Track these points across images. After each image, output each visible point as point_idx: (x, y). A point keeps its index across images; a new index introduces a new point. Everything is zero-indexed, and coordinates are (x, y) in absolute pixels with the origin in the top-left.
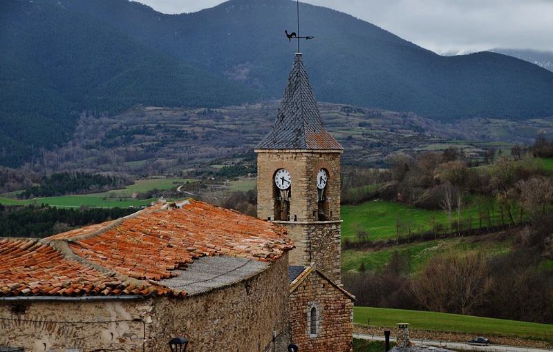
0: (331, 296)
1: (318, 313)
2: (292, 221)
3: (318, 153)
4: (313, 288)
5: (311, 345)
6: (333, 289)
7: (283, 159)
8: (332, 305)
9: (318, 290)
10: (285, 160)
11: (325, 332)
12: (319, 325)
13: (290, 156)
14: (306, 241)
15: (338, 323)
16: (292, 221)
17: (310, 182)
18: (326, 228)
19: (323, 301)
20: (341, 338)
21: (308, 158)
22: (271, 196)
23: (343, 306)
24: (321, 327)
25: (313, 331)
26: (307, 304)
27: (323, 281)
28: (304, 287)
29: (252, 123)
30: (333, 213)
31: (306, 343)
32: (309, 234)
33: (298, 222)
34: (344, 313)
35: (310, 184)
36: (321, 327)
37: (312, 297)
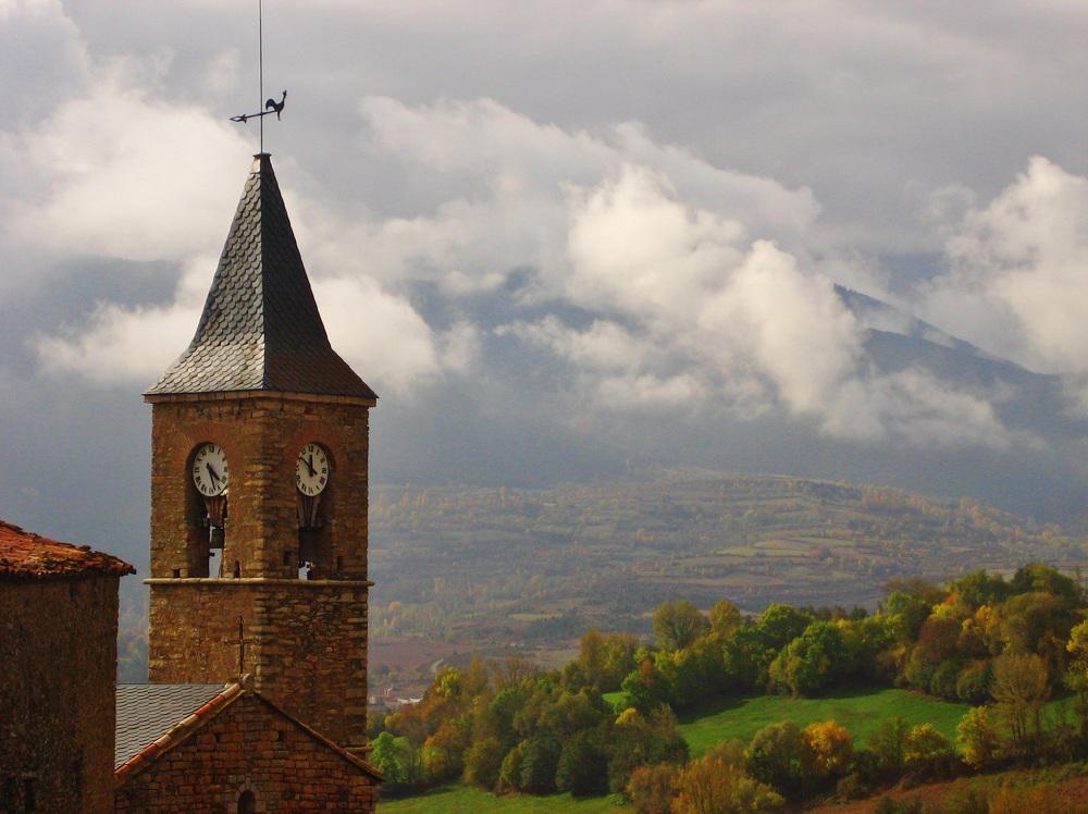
0: (306, 764)
6: (308, 746)
8: (308, 788)
9: (260, 746)
10: (216, 420)
13: (225, 409)
14: (260, 629)
17: (276, 475)
18: (322, 599)
21: (270, 413)
27: (279, 725)
28: (218, 735)
29: (607, 520)
30: (346, 562)
32: (269, 609)
35: (275, 481)
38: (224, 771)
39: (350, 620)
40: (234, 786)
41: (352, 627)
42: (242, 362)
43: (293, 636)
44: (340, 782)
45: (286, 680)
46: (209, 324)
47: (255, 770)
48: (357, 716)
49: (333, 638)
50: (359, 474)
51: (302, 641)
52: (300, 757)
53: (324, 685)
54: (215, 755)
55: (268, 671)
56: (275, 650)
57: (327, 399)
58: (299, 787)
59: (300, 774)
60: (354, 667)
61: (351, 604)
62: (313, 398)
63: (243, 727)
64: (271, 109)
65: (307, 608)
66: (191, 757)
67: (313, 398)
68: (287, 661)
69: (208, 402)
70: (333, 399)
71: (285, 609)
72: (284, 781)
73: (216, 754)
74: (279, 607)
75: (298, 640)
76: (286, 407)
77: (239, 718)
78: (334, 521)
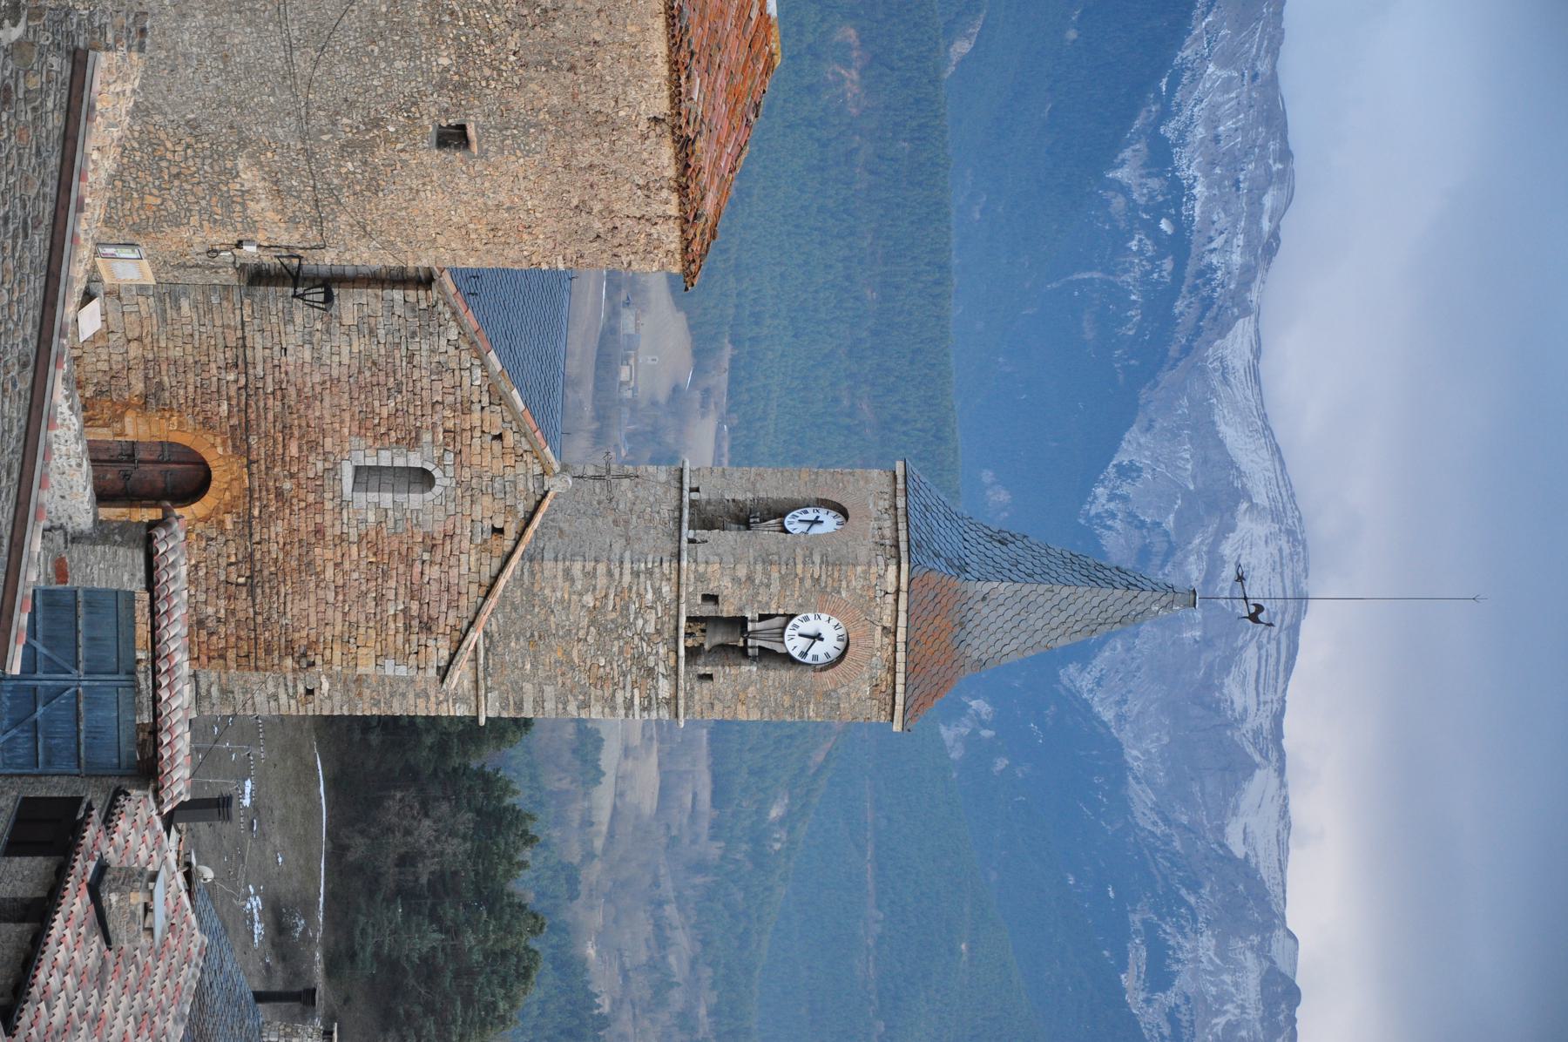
0: (464, 570)
1: (415, 499)
2: (687, 533)
5: (320, 465)
9: (487, 500)
10: (874, 524)
16: (687, 533)
17: (808, 583)
18: (662, 650)
20: (330, 612)
22: (762, 494)
23: (427, 627)
24: (371, 518)
25: (365, 476)
28: (499, 437)
31: (328, 441)
35: (802, 580)
38: (458, 446)
39: (636, 692)
40: (440, 462)
41: (628, 695)
42: (942, 553)
43: (618, 607)
44: (442, 620)
45: (566, 596)
46: (990, 533)
47: (459, 491)
48: (522, 703)
49: (615, 666)
50: (812, 706)
51: (612, 621)
52: (473, 559)
53: (559, 654)
54: (477, 433)
57: (901, 656)
58: (438, 559)
59: (453, 561)
60: (581, 697)
61: (657, 694)
62: (901, 636)
63: (509, 477)
64: (1253, 609)
65: (650, 629)
66: (475, 398)
67: (901, 636)
68: (589, 600)
69: (896, 516)
70: (901, 667)
71: (650, 596)
72: (445, 536)
73: (479, 434)
74: (652, 586)
75: (614, 615)
76: (890, 599)
77: (520, 468)
78: (755, 669)
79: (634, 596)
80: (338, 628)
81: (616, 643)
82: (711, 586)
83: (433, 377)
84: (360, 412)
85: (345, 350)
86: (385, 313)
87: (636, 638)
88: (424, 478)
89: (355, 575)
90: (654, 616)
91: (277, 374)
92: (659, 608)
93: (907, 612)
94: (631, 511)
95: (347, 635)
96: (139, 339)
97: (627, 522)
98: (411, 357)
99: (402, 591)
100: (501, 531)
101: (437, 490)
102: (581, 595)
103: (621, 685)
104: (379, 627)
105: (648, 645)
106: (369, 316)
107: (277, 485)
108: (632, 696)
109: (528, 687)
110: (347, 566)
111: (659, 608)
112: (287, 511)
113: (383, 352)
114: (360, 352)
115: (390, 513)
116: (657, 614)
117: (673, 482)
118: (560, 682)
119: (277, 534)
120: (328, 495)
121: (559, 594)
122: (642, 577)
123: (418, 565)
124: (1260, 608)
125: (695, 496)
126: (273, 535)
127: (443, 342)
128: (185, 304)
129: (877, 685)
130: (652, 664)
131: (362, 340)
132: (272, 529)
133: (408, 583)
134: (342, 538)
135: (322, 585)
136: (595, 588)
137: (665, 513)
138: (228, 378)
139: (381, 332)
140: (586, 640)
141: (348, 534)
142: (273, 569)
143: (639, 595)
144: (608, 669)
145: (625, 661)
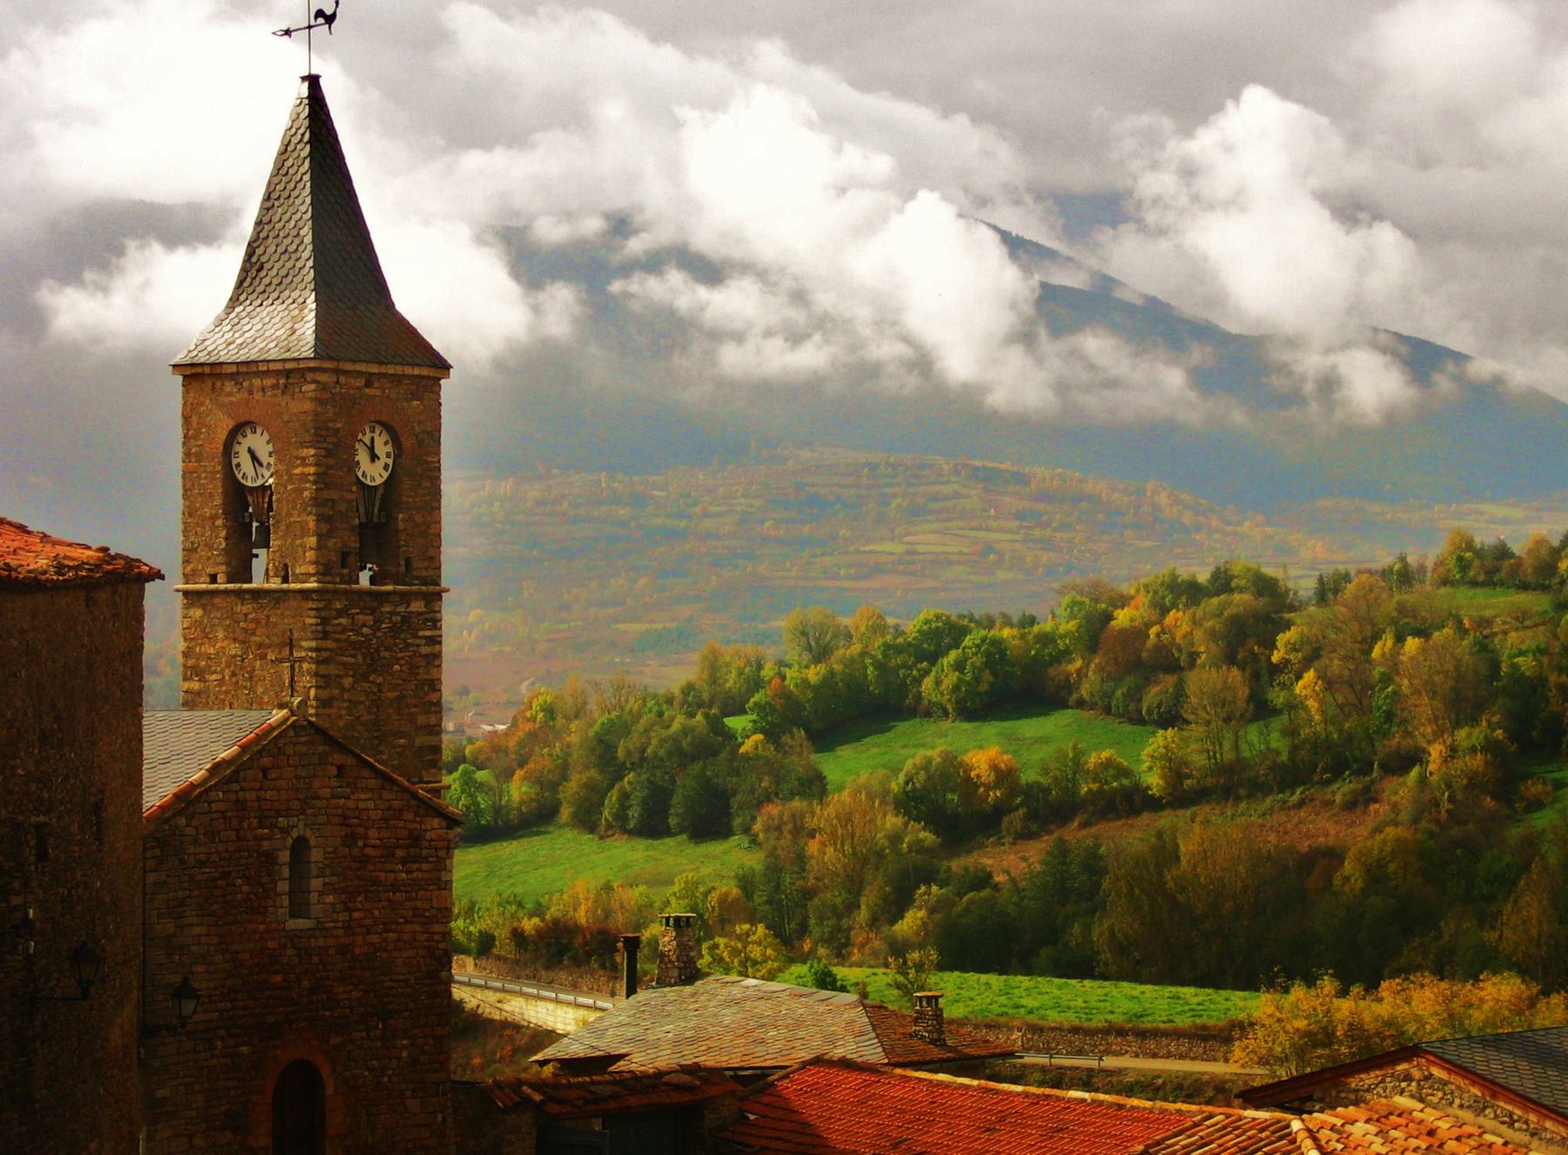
0: (371, 804)
1: (316, 855)
3: (359, 374)
4: (299, 778)
5: (290, 952)
6: (373, 783)
7: (251, 392)
8: (373, 833)
9: (316, 783)
10: (258, 396)
11: (343, 916)
12: (321, 893)
13: (269, 382)
14: (313, 644)
15: (395, 887)
17: (331, 461)
18: (387, 608)
19: (336, 820)
20: (406, 937)
21: (323, 387)
23: (415, 839)
24: (330, 899)
26: (272, 826)
27: (338, 758)
28: (265, 771)
30: (415, 564)
31: (271, 944)
32: (324, 621)
33: (293, 586)
34: (417, 859)
35: (329, 467)
36: (330, 899)
37: (295, 804)
38: (273, 813)
39: (421, 633)
40: (286, 831)
44: (412, 826)
47: (309, 811)
50: (430, 459)
52: (363, 796)
55: (325, 694)
56: (331, 670)
57: (391, 370)
58: (361, 830)
62: (374, 369)
64: (320, 20)
65: (369, 619)
66: (233, 797)
67: (374, 369)
68: (348, 681)
69: (247, 373)
70: (399, 370)
71: (343, 621)
75: (360, 658)
76: (342, 379)
77: (290, 750)
79: (344, 637)
80: (418, 927)
81: (382, 654)
82: (334, 559)
83: (217, 840)
84: (246, 913)
85: (196, 930)
86: (165, 891)
87: (379, 634)
88: (300, 846)
89: (376, 913)
90: (361, 616)
91: (216, 998)
92: (354, 611)
93: (354, 362)
94: (244, 642)
95: (424, 920)
96: (190, 1137)
97: (260, 646)
98: (202, 864)
99: (387, 867)
100: (340, 768)
101: (308, 834)
102: (343, 690)
103: (415, 648)
104: (416, 888)
105: (383, 622)
106: (168, 907)
107: (305, 993)
108: (425, 637)
109: (418, 741)
110: (368, 922)
111: (354, 611)
112: (327, 982)
113: (196, 893)
114: (197, 916)
115: (327, 880)
116: (358, 614)
117: (203, 601)
118: (414, 710)
119: (345, 992)
120: (313, 943)
121: (343, 712)
122: (329, 628)
123: (368, 851)
124: (320, 13)
125: (220, 578)
126: (345, 996)
127: (189, 831)
128: (161, 1093)
129: (412, 394)
130: (399, 618)
131: (187, 914)
132: (341, 997)
133: (382, 860)
134: (348, 928)
135: (383, 944)
136: (338, 676)
137: (247, 608)
138: (220, 1047)
139: (181, 894)
140: (379, 684)
141: (343, 922)
142: (372, 995)
143: (343, 632)
144: (403, 662)
145: (396, 645)
